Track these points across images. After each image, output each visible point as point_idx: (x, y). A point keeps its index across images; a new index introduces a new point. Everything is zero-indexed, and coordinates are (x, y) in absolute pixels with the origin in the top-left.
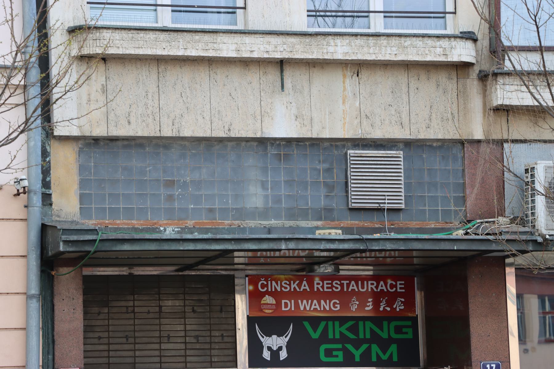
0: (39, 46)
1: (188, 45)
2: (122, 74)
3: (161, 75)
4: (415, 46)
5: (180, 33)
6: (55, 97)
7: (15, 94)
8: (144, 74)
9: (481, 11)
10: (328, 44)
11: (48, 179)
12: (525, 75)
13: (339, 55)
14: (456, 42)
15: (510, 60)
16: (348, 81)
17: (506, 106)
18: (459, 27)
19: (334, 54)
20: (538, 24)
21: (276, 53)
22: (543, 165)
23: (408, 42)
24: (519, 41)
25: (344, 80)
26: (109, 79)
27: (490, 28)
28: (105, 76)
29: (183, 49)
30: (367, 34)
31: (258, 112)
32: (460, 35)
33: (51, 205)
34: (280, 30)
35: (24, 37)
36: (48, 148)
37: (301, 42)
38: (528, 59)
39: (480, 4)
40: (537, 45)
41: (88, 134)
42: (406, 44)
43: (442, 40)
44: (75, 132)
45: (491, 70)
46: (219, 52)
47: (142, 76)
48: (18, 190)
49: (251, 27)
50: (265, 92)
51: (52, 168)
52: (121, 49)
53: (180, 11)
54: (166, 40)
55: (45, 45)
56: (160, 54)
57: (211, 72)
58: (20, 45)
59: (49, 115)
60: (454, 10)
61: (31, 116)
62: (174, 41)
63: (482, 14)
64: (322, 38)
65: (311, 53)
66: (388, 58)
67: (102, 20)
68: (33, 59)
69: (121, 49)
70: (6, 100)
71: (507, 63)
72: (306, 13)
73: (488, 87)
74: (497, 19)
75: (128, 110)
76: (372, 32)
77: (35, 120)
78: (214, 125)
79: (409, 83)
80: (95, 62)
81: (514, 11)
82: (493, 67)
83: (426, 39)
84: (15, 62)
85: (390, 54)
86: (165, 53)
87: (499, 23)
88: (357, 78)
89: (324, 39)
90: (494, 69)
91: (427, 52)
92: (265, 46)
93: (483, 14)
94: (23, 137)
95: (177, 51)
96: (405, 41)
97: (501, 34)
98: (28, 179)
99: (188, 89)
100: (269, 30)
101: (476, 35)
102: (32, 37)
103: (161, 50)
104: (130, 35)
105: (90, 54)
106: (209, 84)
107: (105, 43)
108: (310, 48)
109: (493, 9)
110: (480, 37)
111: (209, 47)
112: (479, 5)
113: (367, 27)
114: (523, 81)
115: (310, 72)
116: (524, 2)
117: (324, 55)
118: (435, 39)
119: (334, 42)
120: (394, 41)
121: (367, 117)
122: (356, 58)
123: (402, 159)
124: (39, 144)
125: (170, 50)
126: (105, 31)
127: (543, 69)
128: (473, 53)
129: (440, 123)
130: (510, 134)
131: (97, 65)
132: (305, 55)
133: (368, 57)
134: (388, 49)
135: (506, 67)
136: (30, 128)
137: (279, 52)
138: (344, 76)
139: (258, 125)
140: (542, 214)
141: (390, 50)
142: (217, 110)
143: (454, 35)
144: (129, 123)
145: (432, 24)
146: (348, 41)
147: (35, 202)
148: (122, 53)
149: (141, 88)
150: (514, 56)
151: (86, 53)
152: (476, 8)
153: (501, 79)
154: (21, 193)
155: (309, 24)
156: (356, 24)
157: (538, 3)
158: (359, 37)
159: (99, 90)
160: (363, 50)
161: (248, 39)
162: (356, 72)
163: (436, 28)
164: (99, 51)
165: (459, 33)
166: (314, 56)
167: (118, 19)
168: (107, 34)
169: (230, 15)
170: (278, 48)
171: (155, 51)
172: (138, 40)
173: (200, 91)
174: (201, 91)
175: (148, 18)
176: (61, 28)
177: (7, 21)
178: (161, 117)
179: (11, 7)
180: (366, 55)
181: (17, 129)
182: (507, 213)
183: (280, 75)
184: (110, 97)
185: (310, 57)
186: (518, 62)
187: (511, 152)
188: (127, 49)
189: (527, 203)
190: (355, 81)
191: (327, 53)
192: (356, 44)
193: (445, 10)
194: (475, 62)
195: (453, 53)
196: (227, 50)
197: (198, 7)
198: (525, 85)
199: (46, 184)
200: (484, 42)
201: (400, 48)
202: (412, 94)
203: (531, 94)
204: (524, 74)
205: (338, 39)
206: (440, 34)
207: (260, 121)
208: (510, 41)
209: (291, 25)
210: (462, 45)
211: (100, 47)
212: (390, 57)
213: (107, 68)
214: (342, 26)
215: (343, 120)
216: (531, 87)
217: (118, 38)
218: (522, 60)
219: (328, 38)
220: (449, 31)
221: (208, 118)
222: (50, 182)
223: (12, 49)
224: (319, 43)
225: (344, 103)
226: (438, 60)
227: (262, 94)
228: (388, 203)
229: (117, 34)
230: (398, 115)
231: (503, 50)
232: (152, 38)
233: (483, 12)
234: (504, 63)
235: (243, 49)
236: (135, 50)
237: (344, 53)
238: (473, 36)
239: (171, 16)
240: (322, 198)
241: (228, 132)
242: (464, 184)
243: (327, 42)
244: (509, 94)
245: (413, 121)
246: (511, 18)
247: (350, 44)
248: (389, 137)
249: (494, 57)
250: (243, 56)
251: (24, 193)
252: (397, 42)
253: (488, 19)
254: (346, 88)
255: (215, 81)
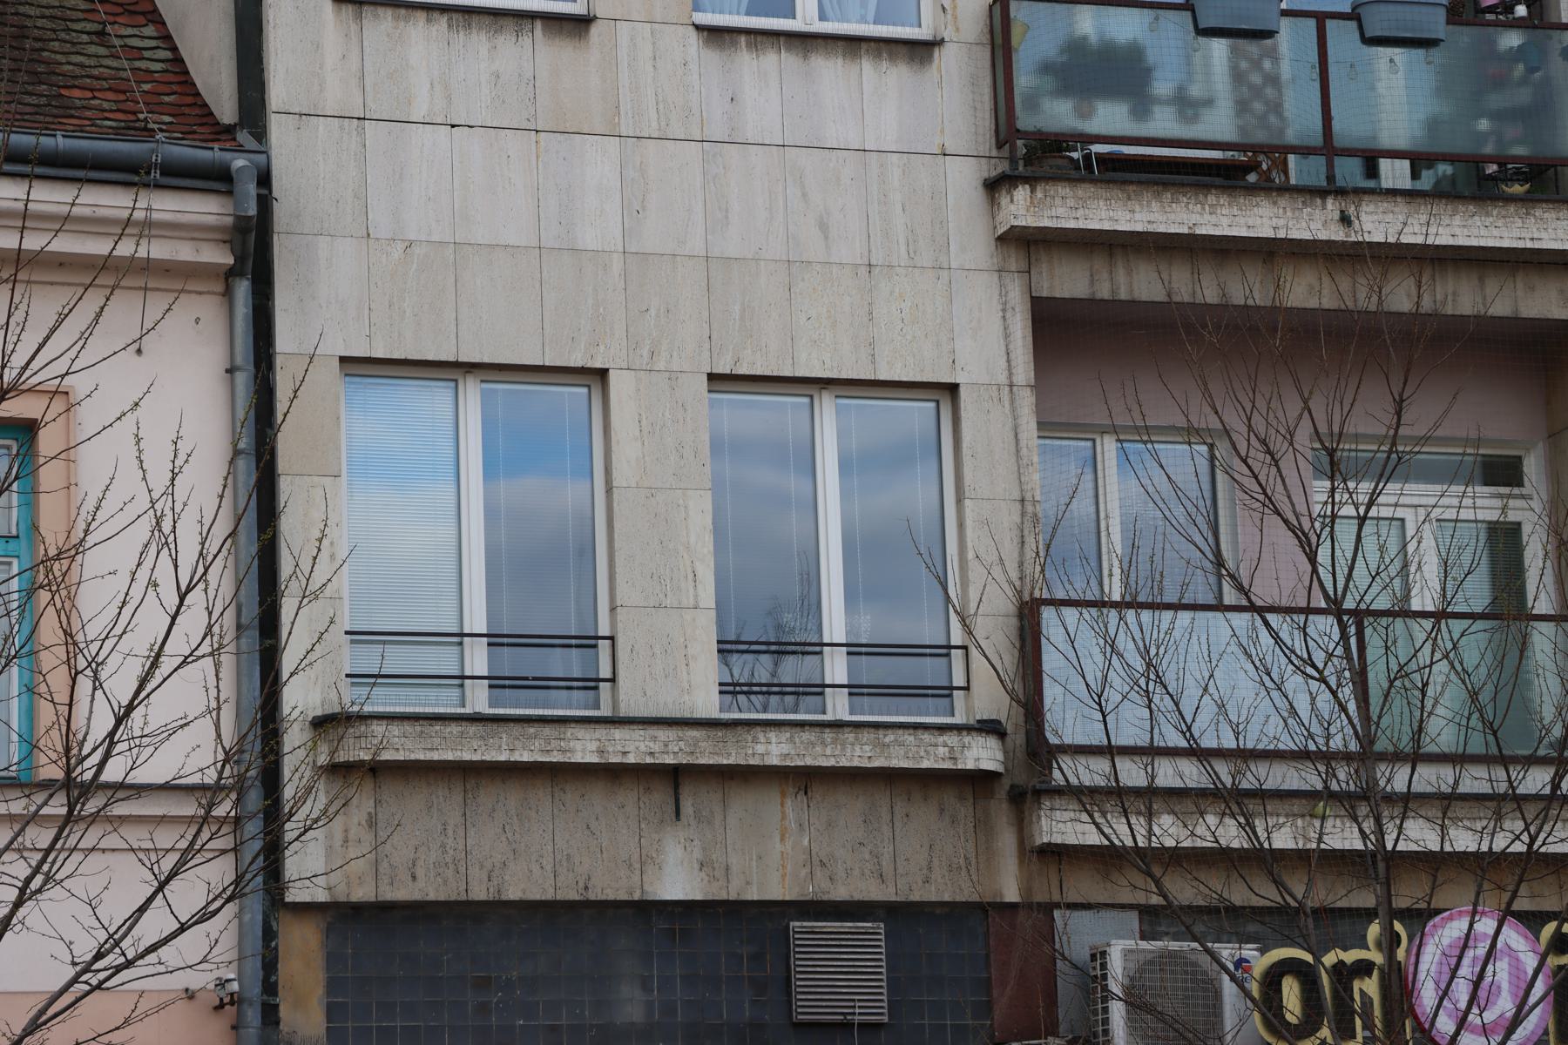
0: (263, 749)
1: (517, 742)
3: (470, 795)
5: (502, 724)
6: (289, 837)
7: (218, 835)
8: (440, 794)
10: (755, 741)
11: (273, 979)
15: (1060, 769)
16: (789, 802)
17: (1057, 845)
19: (765, 757)
21: (666, 756)
22: (1120, 947)
27: (1025, 715)
31: (637, 856)
32: (977, 726)
33: (277, 1023)
35: (239, 731)
36: (274, 924)
37: (709, 737)
41: (342, 899)
42: (887, 740)
44: (322, 896)
46: (569, 755)
47: (438, 797)
48: (221, 999)
51: (280, 960)
52: (402, 752)
53: (504, 687)
55: (272, 750)
57: (556, 789)
58: (231, 750)
59: (277, 867)
61: (246, 872)
68: (252, 773)
69: (402, 752)
70: (204, 845)
71: (1056, 774)
72: (717, 689)
73: (1026, 813)
75: (412, 856)
77: (255, 876)
78: (561, 878)
83: (920, 732)
84: (220, 778)
86: (476, 757)
89: (748, 731)
90: (1035, 782)
91: (922, 754)
94: (231, 909)
96: (885, 736)
98: (240, 979)
102: (251, 737)
104: (418, 728)
107: (375, 742)
110: (1009, 730)
118: (936, 733)
120: (867, 735)
121: (822, 864)
123: (882, 937)
124: (260, 917)
126: (375, 722)
127: (1114, 784)
128: (1000, 756)
129: (947, 874)
130: (1064, 895)
134: (857, 748)
136: (244, 891)
138: (783, 795)
139: (636, 878)
140: (1121, 1033)
142: (565, 853)
144: (414, 878)
146: (788, 735)
147: (249, 1019)
150: (1066, 762)
152: (1001, 681)
154: (227, 1004)
156: (802, 706)
158: (807, 728)
159: (364, 822)
161: (618, 733)
162: (803, 788)
166: (731, 761)
168: (378, 728)
170: (670, 747)
176: (301, 718)
177: (210, 712)
178: (470, 868)
179: (218, 687)
181: (221, 893)
182: (1062, 1028)
184: (381, 833)
185: (725, 762)
187: (1066, 924)
189: (1095, 1013)
190: (802, 802)
191: (754, 755)
193: (951, 682)
196: (583, 751)
197: (535, 679)
199: (270, 988)
200: (1018, 739)
202: (898, 824)
203: (1097, 826)
207: (638, 872)
215: (781, 870)
216: (1096, 815)
217: (396, 733)
218: (1081, 770)
220: (958, 719)
221: (549, 868)
222: (276, 983)
223: (216, 758)
225: (782, 840)
226: (941, 767)
227: (643, 826)
228: (860, 1014)
230: (876, 860)
234: (1051, 773)
235: (611, 749)
240: (747, 1005)
241: (583, 892)
242: (989, 979)
244: (1060, 825)
245: (900, 870)
246: (1060, 699)
247: (791, 740)
248: (861, 899)
251: (232, 1003)
252: (872, 735)
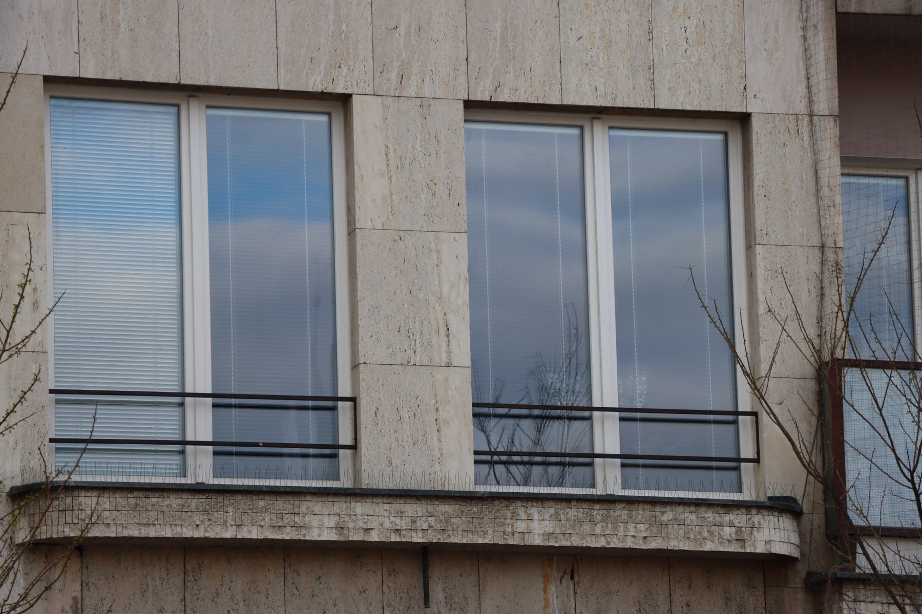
1: (244, 517)
2: (113, 577)
3: (191, 578)
4: (682, 522)
9: (808, 460)
12: (895, 585)
13: (536, 537)
14: (761, 517)
15: (866, 554)
16: (552, 588)
18: (767, 487)
19: (527, 536)
20: (917, 486)
21: (414, 534)
23: (668, 515)
24: (882, 517)
25: (546, 586)
26: (88, 587)
27: (825, 492)
28: (80, 581)
29: (234, 527)
30: (589, 498)
32: (768, 504)
34: (423, 488)
37: (462, 512)
38: (901, 554)
39: (804, 444)
40: (917, 527)
42: (665, 518)
43: (734, 512)
45: (831, 572)
46: (303, 531)
47: (154, 579)
49: (365, 484)
50: (392, 609)
52: (113, 528)
53: (230, 454)
54: (201, 509)
56: (190, 536)
60: (756, 455)
62: (217, 512)
63: (809, 465)
64: (503, 505)
65: (482, 533)
66: (629, 544)
67: (78, 473)
69: (113, 528)
71: (861, 560)
72: (471, 458)
73: (826, 606)
74: (839, 475)
76: (599, 493)
79: (672, 593)
80: (63, 557)
81: (871, 462)
82: (835, 566)
83: (702, 509)
85: (633, 536)
87: (842, 481)
88: (571, 583)
89: (507, 507)
90: (835, 569)
91: (705, 534)
92: (392, 519)
93: (811, 463)
95: (223, 531)
96: (663, 513)
97: (848, 503)
99: (242, 604)
100: (401, 488)
101: (798, 504)
103: (190, 528)
104: (132, 501)
105: (51, 538)
106: (283, 593)
108: (479, 524)
109: (831, 454)
110: (806, 507)
111: (285, 521)
112: (803, 447)
113: (589, 483)
114: (892, 597)
115: (480, 569)
116: (889, 446)
117: (507, 537)
118: (721, 511)
119: (526, 512)
120: (642, 513)
122: (569, 544)
125: (208, 529)
128: (795, 539)
131: (66, 564)
132: (471, 536)
133: (592, 541)
134: (631, 527)
135: (859, 567)
137: (421, 532)
138: (546, 579)
141: (633, 530)
143: (756, 502)
145: (715, 480)
146: (552, 511)
148: (115, 536)
149: (149, 603)
150: (873, 547)
151: (45, 537)
152: (797, 453)
153: (850, 590)
155: (478, 478)
156: (568, 479)
157: (916, 448)
158: (574, 503)
159: (68, 609)
160: (582, 528)
161: (359, 507)
162: (568, 571)
163: (722, 490)
164: (71, 532)
165: (766, 500)
167: (109, 470)
168: (88, 501)
169: (326, 460)
170: (418, 523)
171: (180, 531)
172: (147, 510)
173: (266, 607)
174: (268, 607)
175: (168, 467)
180: (588, 539)
183: (422, 576)
185: (481, 541)
186: (881, 559)
188: (126, 527)
190: (568, 587)
191: (513, 533)
192: (568, 516)
194: (799, 557)
195: (755, 538)
196: (320, 527)
197: (266, 445)
198: (897, 603)
200: (815, 519)
201: (653, 526)
204: (894, 581)
205: (533, 506)
206: (730, 500)
208: (866, 518)
209: (443, 479)
210: (772, 523)
211: (72, 525)
212: (633, 542)
213: (85, 565)
214: (542, 482)
217: (107, 506)
218: (890, 556)
219: (514, 504)
220: (747, 495)
224: (497, 515)
226: (726, 550)
229: (105, 500)
231: (852, 535)
232: (175, 506)
233: (811, 460)
234: (855, 559)
235: (351, 525)
236: (140, 530)
237: (544, 534)
238: (793, 505)
239: (212, 463)
243: (513, 513)
246: (865, 474)
247: (556, 517)
249: (835, 548)
250: (350, 539)
253: (821, 474)
254: (549, 602)
255: (294, 587)
